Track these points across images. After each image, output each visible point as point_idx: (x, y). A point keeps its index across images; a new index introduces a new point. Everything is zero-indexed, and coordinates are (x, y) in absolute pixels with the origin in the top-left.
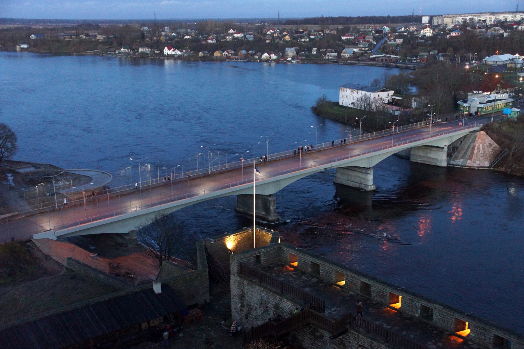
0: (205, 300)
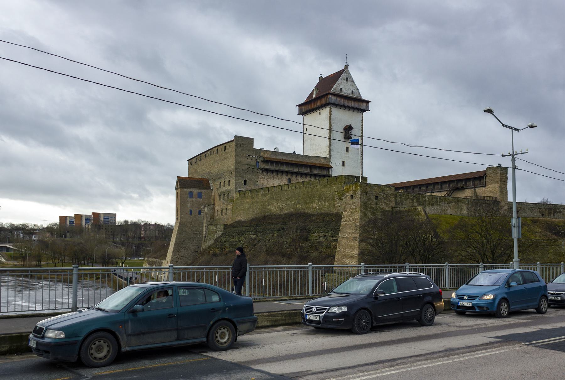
0: (371, 102)
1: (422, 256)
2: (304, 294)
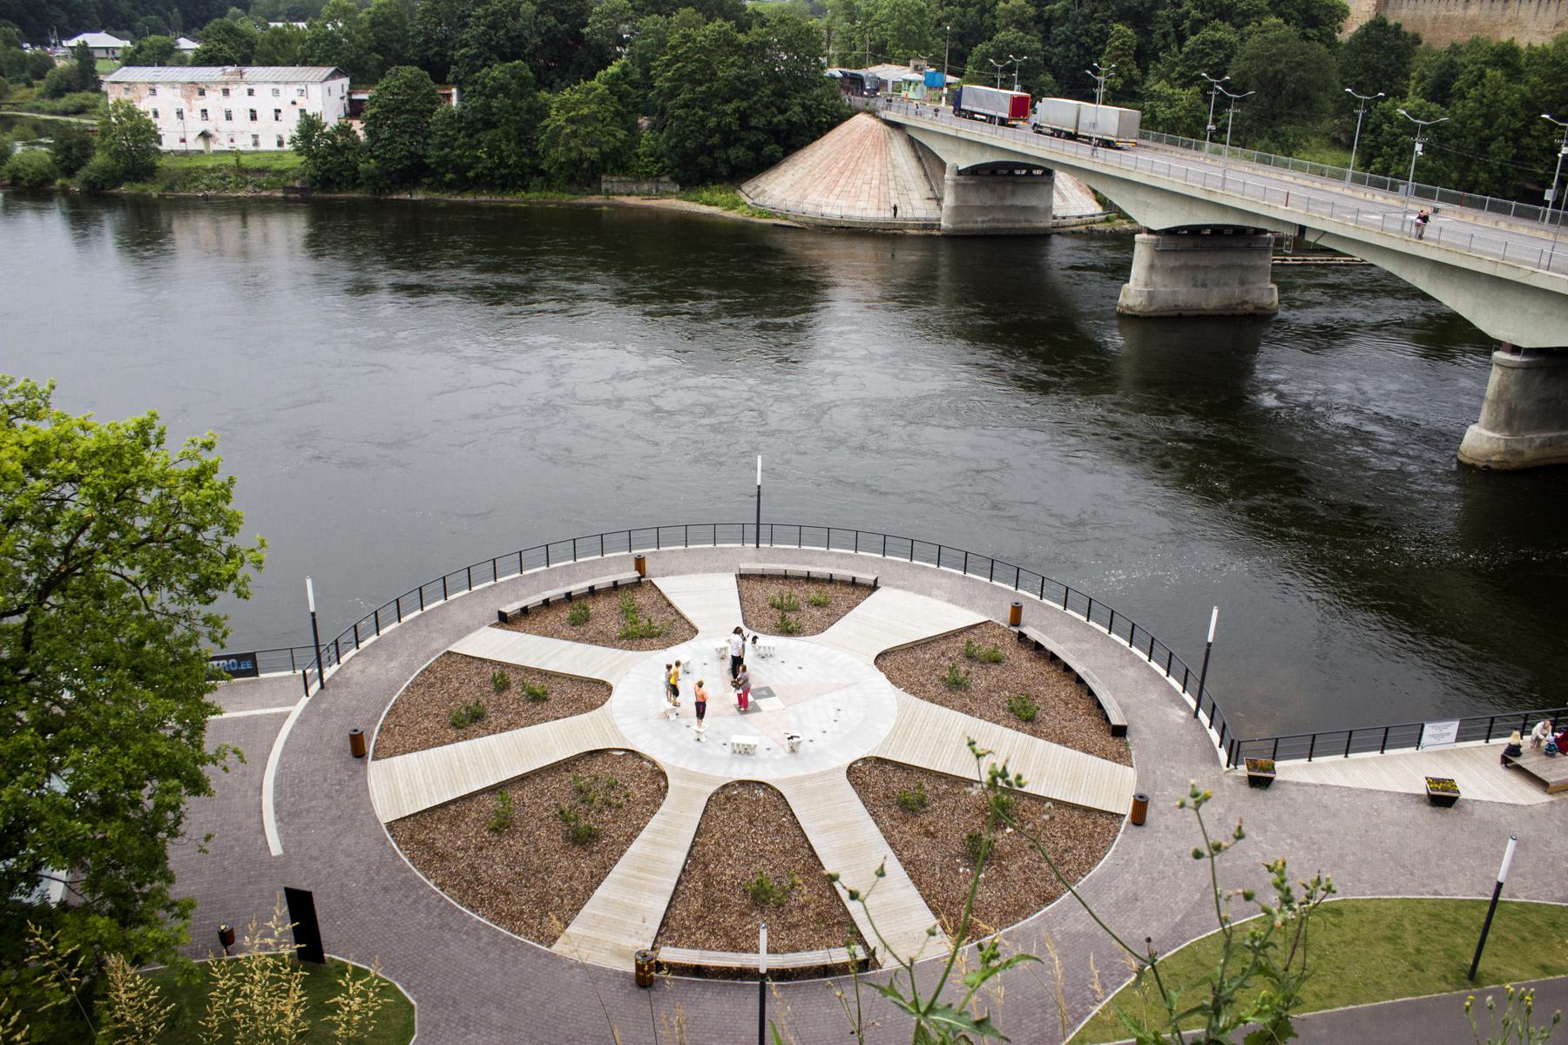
1: (651, 403)
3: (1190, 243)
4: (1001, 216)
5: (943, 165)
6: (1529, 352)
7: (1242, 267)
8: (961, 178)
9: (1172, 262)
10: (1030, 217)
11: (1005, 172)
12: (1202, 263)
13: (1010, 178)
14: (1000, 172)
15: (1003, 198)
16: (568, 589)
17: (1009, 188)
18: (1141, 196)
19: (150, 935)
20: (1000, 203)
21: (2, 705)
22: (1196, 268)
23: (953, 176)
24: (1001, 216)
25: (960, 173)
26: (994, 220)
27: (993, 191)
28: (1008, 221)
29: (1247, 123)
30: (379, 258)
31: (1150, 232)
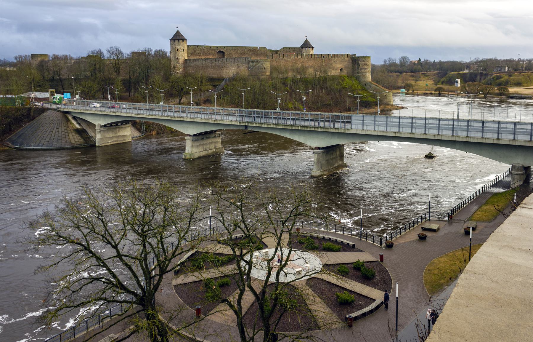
2: (248, 114)
3: (200, 137)
4: (115, 139)
5: (95, 125)
6: (323, 148)
7: (214, 142)
8: (102, 129)
9: (197, 144)
10: (126, 139)
11: (115, 125)
12: (205, 143)
13: (117, 126)
14: (107, 125)
15: (116, 133)
16: (343, 240)
17: (117, 130)
18: (185, 125)
19: (338, 293)
20: (115, 135)
21: (1, 261)
22: (203, 145)
23: (99, 128)
24: (115, 139)
25: (101, 127)
26: (114, 141)
27: (113, 131)
28: (118, 141)
29: (13, 112)
30: (357, 193)
31: (190, 135)
